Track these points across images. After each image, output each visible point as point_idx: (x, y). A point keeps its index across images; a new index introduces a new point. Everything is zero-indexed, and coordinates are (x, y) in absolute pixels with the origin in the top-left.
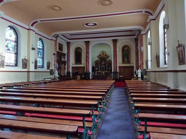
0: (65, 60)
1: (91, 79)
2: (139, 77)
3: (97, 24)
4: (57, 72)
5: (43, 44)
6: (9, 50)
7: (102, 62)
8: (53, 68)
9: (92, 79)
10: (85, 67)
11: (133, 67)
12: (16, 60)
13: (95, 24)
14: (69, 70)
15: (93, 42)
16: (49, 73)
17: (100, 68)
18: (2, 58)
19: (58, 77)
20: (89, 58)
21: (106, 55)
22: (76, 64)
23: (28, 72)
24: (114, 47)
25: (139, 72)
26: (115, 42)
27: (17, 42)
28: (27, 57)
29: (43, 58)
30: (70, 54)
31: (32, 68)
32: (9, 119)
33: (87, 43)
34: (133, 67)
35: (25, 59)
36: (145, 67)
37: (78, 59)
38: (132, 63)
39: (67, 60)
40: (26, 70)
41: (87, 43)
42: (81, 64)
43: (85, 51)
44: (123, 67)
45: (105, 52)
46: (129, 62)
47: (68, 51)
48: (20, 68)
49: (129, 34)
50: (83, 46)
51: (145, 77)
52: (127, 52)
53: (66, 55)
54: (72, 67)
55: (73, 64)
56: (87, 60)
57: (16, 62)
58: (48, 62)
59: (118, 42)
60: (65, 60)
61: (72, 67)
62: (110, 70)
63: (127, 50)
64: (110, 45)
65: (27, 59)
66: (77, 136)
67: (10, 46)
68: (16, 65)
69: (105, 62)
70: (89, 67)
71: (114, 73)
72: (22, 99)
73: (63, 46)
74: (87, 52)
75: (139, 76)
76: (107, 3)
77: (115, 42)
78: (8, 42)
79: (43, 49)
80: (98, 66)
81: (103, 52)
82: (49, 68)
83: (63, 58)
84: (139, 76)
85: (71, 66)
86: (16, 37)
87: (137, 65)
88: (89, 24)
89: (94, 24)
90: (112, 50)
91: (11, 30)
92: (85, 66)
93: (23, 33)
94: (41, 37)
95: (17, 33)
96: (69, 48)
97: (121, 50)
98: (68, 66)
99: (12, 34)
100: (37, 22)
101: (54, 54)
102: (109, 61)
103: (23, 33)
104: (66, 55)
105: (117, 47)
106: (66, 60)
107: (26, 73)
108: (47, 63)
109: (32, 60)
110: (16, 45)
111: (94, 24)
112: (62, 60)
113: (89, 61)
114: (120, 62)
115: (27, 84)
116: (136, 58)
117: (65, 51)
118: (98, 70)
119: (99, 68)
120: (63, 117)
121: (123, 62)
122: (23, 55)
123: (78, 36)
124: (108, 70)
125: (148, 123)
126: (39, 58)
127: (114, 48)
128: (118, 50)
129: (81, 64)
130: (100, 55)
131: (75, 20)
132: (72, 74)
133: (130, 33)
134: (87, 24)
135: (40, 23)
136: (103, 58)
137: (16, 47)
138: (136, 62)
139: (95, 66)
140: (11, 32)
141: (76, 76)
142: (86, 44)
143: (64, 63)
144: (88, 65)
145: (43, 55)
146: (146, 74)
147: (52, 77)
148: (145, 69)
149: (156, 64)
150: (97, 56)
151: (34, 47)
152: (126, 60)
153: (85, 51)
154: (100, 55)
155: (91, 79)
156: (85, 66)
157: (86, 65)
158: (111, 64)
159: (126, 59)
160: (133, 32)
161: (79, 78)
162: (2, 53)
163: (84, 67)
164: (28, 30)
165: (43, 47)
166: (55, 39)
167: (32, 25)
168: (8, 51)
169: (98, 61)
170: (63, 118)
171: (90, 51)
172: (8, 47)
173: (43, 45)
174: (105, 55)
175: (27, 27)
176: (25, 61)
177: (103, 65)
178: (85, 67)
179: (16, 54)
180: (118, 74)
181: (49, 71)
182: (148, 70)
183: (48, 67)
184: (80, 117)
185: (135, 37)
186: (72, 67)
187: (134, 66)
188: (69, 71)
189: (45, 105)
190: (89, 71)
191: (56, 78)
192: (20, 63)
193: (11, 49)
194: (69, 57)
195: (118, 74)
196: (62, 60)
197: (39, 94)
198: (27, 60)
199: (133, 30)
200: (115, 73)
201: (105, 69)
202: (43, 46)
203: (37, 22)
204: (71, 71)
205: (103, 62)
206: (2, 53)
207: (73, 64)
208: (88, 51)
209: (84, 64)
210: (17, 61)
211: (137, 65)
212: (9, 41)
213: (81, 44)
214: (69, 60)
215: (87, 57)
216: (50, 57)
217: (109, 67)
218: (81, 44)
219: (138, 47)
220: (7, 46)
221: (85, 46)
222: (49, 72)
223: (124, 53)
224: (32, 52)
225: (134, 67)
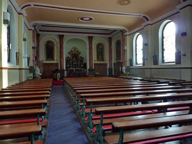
1: (65, 76)
3: (92, 19)
9: (66, 77)
10: (58, 63)
13: (91, 19)
15: (68, 37)
16: (29, 70)
17: (72, 65)
20: (63, 53)
21: (78, 52)
23: (20, 69)
26: (90, 38)
30: (40, 48)
32: (7, 129)
33: (61, 37)
38: (106, 61)
40: (18, 67)
41: (61, 37)
42: (53, 60)
43: (59, 45)
47: (37, 45)
49: (104, 33)
50: (55, 40)
52: (101, 50)
59: (93, 39)
62: (82, 67)
63: (102, 48)
64: (85, 42)
66: (45, 138)
70: (63, 65)
72: (23, 102)
76: (126, 2)
77: (90, 38)
80: (69, 63)
81: (75, 48)
87: (110, 63)
88: (84, 19)
89: (89, 19)
90: (88, 46)
96: (39, 40)
97: (96, 48)
100: (30, 5)
107: (18, 70)
111: (89, 19)
114: (95, 60)
115: (21, 83)
119: (71, 65)
120: (107, 116)
123: (68, 29)
125: (104, 116)
128: (93, 47)
129: (53, 60)
131: (60, 10)
134: (82, 19)
135: (33, 8)
136: (75, 54)
138: (109, 59)
142: (89, 40)
151: (25, 37)
152: (100, 57)
153: (58, 45)
155: (65, 76)
160: (108, 31)
161: (59, 75)
163: (57, 64)
164: (19, 14)
170: (97, 118)
171: (64, 45)
174: (77, 51)
178: (58, 63)
182: (131, 67)
184: (99, 116)
185: (109, 36)
187: (107, 64)
189: (127, 103)
197: (118, 92)
199: (108, 30)
201: (77, 66)
203: (30, 5)
205: (75, 58)
208: (62, 46)
211: (110, 63)
213: (53, 37)
214: (39, 55)
215: (61, 53)
218: (55, 38)
219: (111, 46)
221: (58, 40)
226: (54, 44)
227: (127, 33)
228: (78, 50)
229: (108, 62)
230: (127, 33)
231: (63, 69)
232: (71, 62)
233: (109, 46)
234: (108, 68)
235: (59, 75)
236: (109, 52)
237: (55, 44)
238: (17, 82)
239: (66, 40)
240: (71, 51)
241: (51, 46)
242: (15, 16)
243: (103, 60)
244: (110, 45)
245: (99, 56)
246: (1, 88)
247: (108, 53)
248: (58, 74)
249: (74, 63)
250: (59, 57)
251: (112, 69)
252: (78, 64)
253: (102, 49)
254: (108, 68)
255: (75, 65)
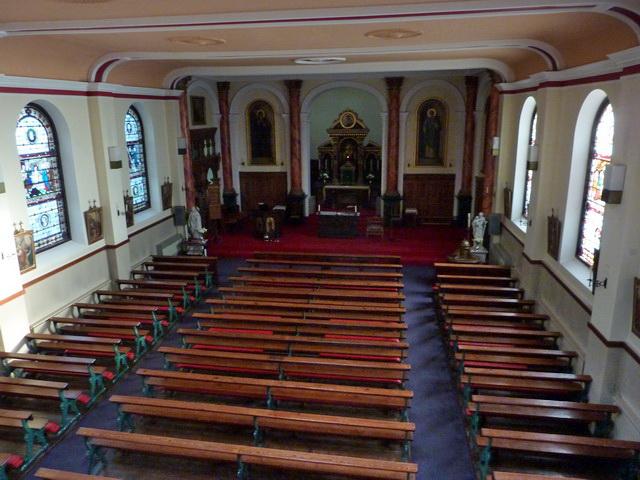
0: (214, 153)
2: (478, 243)
4: (196, 215)
5: (140, 121)
6: (35, 192)
7: (342, 149)
8: (183, 203)
10: (285, 174)
11: (452, 177)
12: (63, 219)
14: (232, 184)
17: (339, 172)
18: (23, 240)
19: (205, 236)
20: (299, 142)
21: (361, 127)
22: (253, 162)
23: (107, 247)
24: (389, 106)
25: (478, 223)
27: (55, 152)
28: (97, 199)
29: (145, 175)
30: (231, 125)
31: (119, 230)
34: (452, 177)
35: (91, 210)
36: (498, 209)
37: (261, 147)
38: (451, 165)
39: (223, 148)
40: (101, 244)
43: (286, 116)
44: (417, 177)
45: (356, 114)
46: (439, 160)
47: (223, 117)
48: (79, 246)
51: (495, 239)
52: (436, 126)
53: (218, 133)
54: (242, 175)
55: (243, 164)
56: (292, 153)
57: (63, 226)
58: (163, 184)
60: (214, 153)
61: (240, 173)
63: (437, 118)
65: (98, 205)
67: (36, 177)
68: (67, 236)
69: (356, 150)
71: (386, 198)
73: (206, 103)
74: (294, 123)
75: (479, 237)
78: (28, 166)
79: (142, 141)
80: (329, 166)
82: (170, 203)
83: (208, 146)
84: (479, 237)
85: (237, 169)
86: (51, 135)
91: (29, 115)
92: (287, 169)
93: (72, 112)
94: (132, 101)
95: (52, 117)
98: (228, 172)
99: (35, 129)
101: (182, 152)
102: (370, 145)
103: (72, 112)
104: (218, 133)
105: (403, 108)
106: (218, 150)
108: (162, 187)
109: (116, 205)
110: (55, 165)
112: (206, 154)
113: (300, 155)
114: (408, 163)
116: (465, 149)
117: (213, 120)
118: (330, 181)
119: (335, 174)
121: (421, 158)
122: (83, 198)
124: (366, 182)
126: (135, 177)
127: (390, 112)
128: (403, 116)
129: (272, 162)
130: (338, 127)
132: (242, 196)
133: (501, 443)
137: (56, 172)
138: (464, 161)
139: (316, 157)
140: (33, 122)
141: (259, 219)
143: (214, 162)
144: (297, 169)
145: (145, 162)
146: (500, 233)
147: (182, 230)
148: (500, 215)
149: (546, 244)
150: (328, 131)
152: (430, 152)
154: (338, 127)
156: (287, 169)
157: (292, 169)
158: (377, 159)
159: (431, 150)
161: (270, 224)
162: (21, 224)
165: (142, 131)
166: (177, 93)
167: (98, 79)
168: (36, 199)
169: (330, 145)
172: (32, 184)
173: (141, 125)
174: (358, 126)
175: (83, 87)
176: (94, 216)
177: (348, 163)
179: (62, 197)
180: (401, 203)
181: (168, 213)
183: (166, 204)
186: (240, 173)
188: (233, 190)
190: (301, 191)
191: (197, 236)
192: (80, 227)
193: (41, 187)
194: (229, 138)
195: (401, 203)
196: (206, 154)
198: (99, 211)
200: (392, 200)
202: (142, 128)
204: (237, 187)
205: (349, 155)
206: (21, 224)
207: (243, 164)
209: (282, 164)
210: (66, 221)
212: (32, 161)
215: (294, 143)
216: (169, 165)
217: (368, 172)
220: (28, 183)
221: (284, 100)
222: (170, 217)
223: (424, 130)
224: (113, 175)
225: (454, 179)
226: (270, 107)
227: (504, 86)
228: (361, 121)
229: (457, 171)
230: (504, 86)
231: (299, 194)
232: (336, 162)
233: (467, 112)
234: (457, 191)
235: (270, 224)
236: (466, 135)
237: (276, 108)
238: (103, 283)
239: (310, 96)
240: (336, 127)
241: (265, 119)
242: (101, 114)
243: (439, 160)
244: (471, 106)
245: (427, 148)
246: (1, 371)
247: (463, 137)
248: (268, 221)
249: (343, 168)
250: (288, 151)
251: (471, 198)
252: (357, 171)
253: (440, 123)
254: (457, 191)
255: (348, 173)
